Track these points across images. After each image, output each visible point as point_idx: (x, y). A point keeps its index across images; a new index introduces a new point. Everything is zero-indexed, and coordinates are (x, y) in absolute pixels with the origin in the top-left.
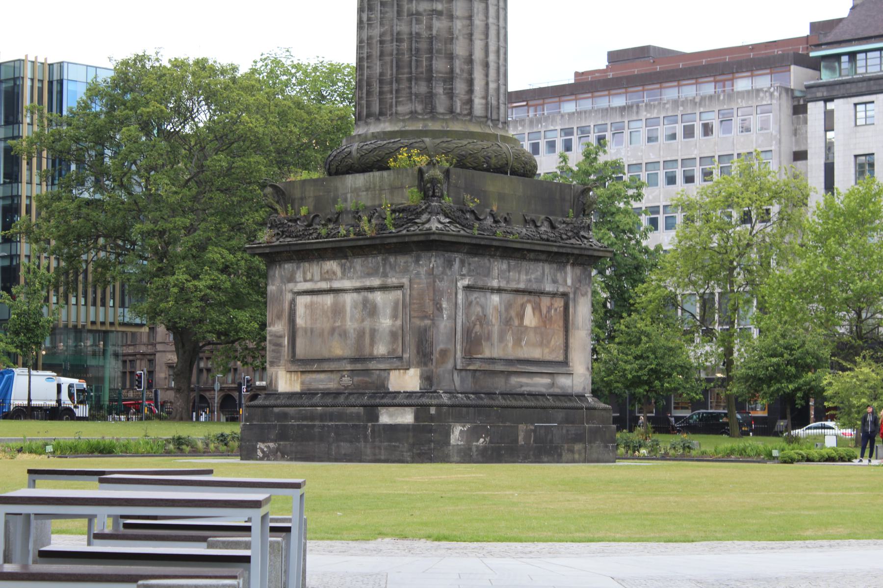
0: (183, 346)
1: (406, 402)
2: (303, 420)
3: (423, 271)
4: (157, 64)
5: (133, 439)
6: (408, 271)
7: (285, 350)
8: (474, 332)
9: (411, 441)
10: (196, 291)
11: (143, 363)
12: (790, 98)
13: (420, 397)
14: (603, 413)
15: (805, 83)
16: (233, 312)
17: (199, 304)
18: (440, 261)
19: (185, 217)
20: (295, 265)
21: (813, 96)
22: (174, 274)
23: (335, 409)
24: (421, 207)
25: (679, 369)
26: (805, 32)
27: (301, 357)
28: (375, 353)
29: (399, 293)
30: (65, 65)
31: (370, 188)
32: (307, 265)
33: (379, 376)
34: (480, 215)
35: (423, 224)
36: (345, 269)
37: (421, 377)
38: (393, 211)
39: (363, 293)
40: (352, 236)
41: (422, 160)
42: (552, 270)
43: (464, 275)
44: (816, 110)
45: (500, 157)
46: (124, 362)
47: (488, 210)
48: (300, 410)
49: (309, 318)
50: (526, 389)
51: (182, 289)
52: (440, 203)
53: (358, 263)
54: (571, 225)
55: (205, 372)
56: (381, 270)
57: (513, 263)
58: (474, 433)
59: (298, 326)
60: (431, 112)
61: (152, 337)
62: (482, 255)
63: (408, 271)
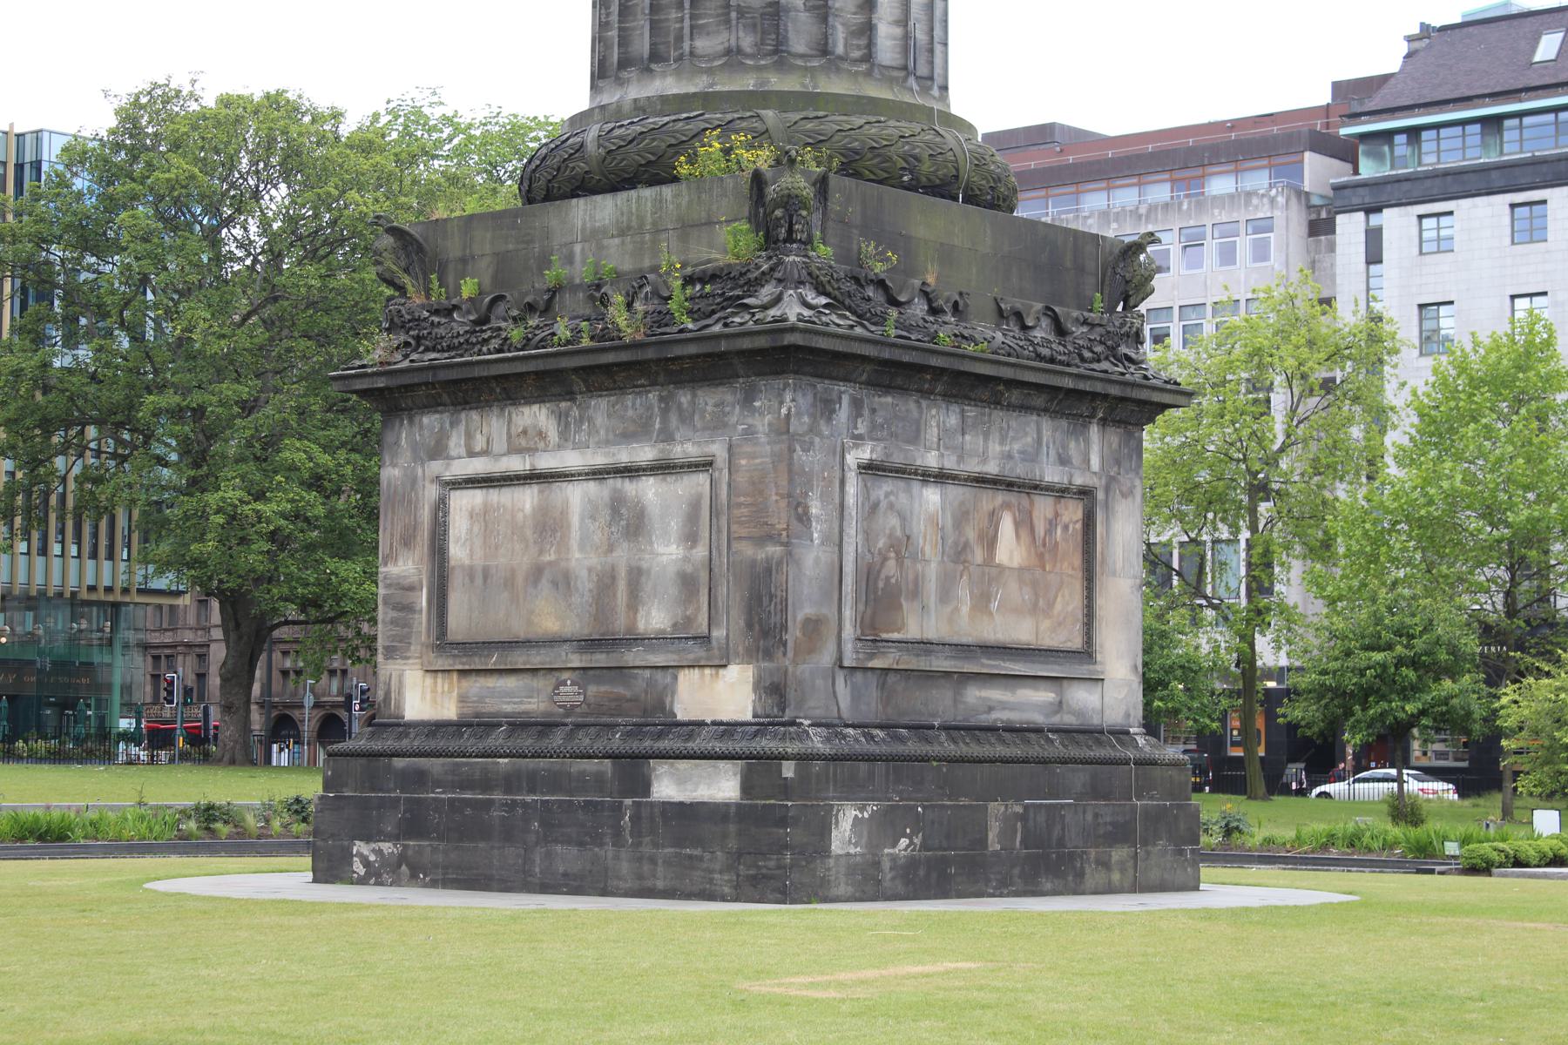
0: (238, 626)
1: (719, 746)
2: (463, 788)
3: (762, 424)
4: (194, 106)
5: (112, 808)
6: (725, 425)
7: (422, 620)
8: (883, 576)
9: (732, 844)
10: (260, 522)
11: (189, 658)
12: (1304, 208)
13: (755, 734)
14: (1173, 772)
15: (1332, 181)
16: (332, 564)
17: (266, 546)
18: (805, 401)
19: (239, 383)
20: (446, 416)
21: (1346, 202)
22: (218, 489)
23: (542, 763)
24: (758, 267)
25: (1179, 672)
26: (1324, 97)
27: (459, 638)
28: (641, 626)
29: (702, 479)
30: (46, 136)
31: (629, 228)
32: (475, 415)
33: (650, 683)
34: (900, 292)
35: (765, 308)
36: (567, 425)
37: (757, 686)
38: (689, 281)
39: (611, 481)
40: (586, 342)
41: (762, 158)
42: (1057, 434)
43: (860, 437)
44: (1351, 228)
45: (940, 158)
46: (156, 658)
47: (917, 283)
48: (457, 764)
49: (478, 542)
50: (1000, 716)
51: (233, 518)
52: (806, 256)
53: (600, 408)
54: (1099, 330)
55: (292, 676)
56: (657, 426)
57: (971, 412)
58: (885, 826)
59: (452, 563)
60: (776, 52)
61: (203, 618)
62: (903, 390)
63: (725, 425)
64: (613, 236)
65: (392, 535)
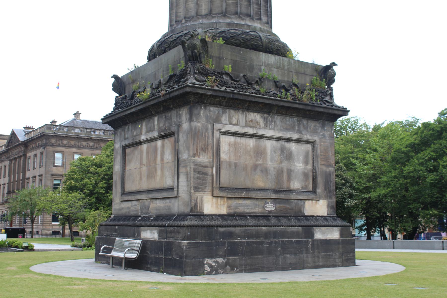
3: (327, 134)
20: (221, 110)
23: (278, 229)
28: (292, 187)
32: (232, 112)
33: (297, 204)
36: (267, 122)
37: (328, 206)
39: (281, 142)
40: (289, 100)
48: (246, 230)
53: (278, 119)
56: (297, 128)
63: (317, 132)
64: (274, 68)
65: (197, 147)
